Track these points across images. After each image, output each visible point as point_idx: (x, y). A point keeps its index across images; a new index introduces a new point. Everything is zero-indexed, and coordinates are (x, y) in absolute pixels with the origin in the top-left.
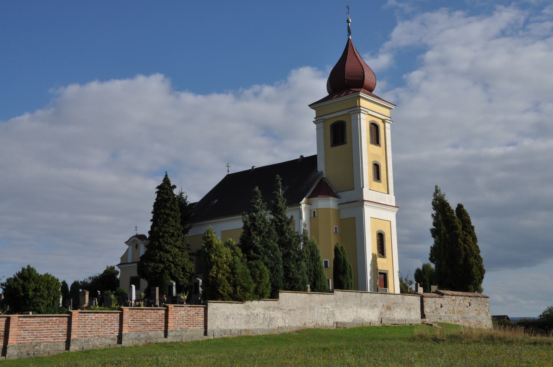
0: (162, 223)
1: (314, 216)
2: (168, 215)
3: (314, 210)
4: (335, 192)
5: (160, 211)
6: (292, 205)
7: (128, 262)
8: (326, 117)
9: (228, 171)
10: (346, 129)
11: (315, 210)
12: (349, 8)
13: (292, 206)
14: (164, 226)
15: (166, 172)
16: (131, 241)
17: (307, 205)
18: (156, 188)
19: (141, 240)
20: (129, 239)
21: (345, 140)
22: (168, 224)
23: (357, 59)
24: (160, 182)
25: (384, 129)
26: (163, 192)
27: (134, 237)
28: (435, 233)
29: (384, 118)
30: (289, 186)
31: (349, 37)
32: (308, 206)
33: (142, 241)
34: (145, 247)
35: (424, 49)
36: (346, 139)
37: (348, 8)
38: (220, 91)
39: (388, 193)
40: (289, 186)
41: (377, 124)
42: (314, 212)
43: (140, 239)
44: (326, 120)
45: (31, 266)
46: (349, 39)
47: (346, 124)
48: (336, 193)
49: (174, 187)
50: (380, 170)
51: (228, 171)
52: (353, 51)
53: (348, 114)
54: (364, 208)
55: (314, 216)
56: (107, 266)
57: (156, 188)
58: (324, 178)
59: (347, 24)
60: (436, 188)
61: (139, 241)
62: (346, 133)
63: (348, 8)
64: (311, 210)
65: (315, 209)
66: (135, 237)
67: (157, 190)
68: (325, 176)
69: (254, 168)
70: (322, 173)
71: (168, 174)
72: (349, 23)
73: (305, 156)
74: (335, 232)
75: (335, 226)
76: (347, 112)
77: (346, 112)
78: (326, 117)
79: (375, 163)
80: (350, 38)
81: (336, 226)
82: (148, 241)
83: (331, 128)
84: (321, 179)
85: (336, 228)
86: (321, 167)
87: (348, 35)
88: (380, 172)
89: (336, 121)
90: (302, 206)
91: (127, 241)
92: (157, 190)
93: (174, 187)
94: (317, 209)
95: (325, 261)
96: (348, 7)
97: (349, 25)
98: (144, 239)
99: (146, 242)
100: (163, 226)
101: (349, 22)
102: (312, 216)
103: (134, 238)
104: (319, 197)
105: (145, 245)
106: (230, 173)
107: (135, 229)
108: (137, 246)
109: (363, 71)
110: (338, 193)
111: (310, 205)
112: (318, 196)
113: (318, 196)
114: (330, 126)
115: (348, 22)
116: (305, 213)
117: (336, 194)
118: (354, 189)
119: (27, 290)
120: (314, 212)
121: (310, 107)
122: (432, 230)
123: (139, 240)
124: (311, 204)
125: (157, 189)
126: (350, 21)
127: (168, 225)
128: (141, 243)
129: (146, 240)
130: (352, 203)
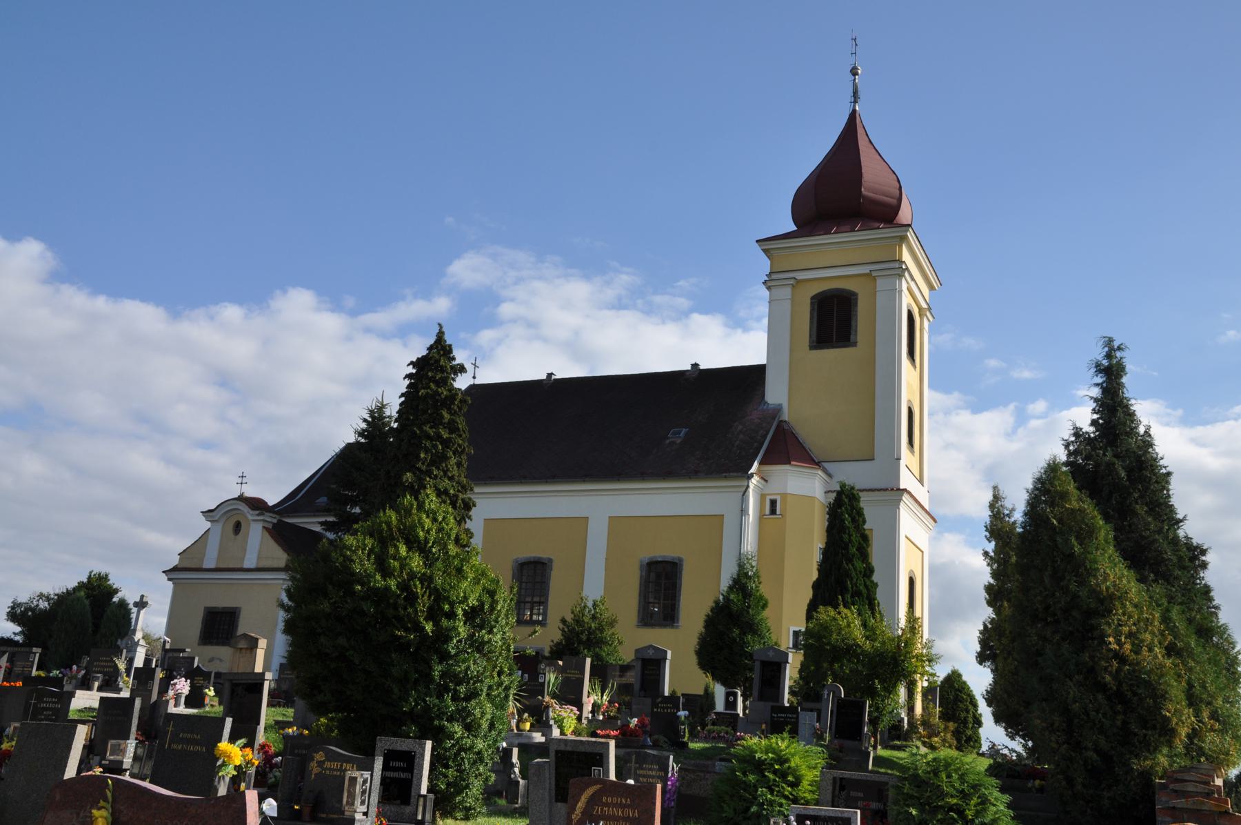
0: (428, 465)
1: (773, 512)
2: (446, 443)
3: (773, 497)
5: (420, 429)
6: (724, 475)
7: (204, 567)
8: (801, 276)
9: (474, 377)
13: (725, 477)
14: (433, 473)
15: (440, 325)
16: (222, 512)
18: (409, 365)
19: (257, 512)
20: (218, 506)
21: (852, 337)
22: (443, 470)
23: (879, 157)
24: (432, 341)
26: (432, 377)
27: (235, 502)
28: (995, 595)
30: (687, 429)
31: (854, 106)
33: (258, 515)
34: (267, 534)
35: (497, 300)
36: (856, 335)
38: (144, 299)
40: (687, 429)
42: (773, 503)
43: (253, 510)
44: (798, 282)
45: (1136, 413)
46: (854, 111)
47: (857, 299)
49: (462, 369)
51: (474, 377)
52: (866, 137)
53: (868, 275)
55: (773, 512)
56: (91, 572)
57: (409, 365)
58: (785, 421)
60: (994, 491)
61: (250, 514)
62: (856, 321)
65: (778, 494)
66: (238, 502)
67: (412, 370)
69: (553, 377)
70: (778, 410)
71: (444, 329)
72: (857, 77)
73: (704, 366)
76: (868, 271)
77: (865, 270)
78: (801, 276)
80: (857, 109)
82: (274, 518)
83: (812, 303)
84: (778, 426)
86: (776, 393)
89: (829, 290)
91: (210, 511)
92: (412, 370)
93: (462, 369)
94: (784, 496)
95: (794, 631)
97: (857, 81)
98: (267, 512)
99: (269, 520)
100: (429, 473)
101: (857, 74)
102: (767, 511)
103: (234, 504)
104: (793, 465)
105: (264, 527)
106: (478, 382)
107: (240, 480)
108: (237, 527)
109: (898, 185)
112: (792, 463)
113: (792, 463)
115: (854, 72)
116: (754, 500)
118: (873, 459)
119: (447, 607)
120: (773, 503)
121: (760, 246)
122: (989, 589)
123: (251, 512)
124: (766, 481)
125: (411, 366)
126: (859, 72)
127: (442, 473)
128: (253, 520)
129: (271, 515)
130: (870, 493)
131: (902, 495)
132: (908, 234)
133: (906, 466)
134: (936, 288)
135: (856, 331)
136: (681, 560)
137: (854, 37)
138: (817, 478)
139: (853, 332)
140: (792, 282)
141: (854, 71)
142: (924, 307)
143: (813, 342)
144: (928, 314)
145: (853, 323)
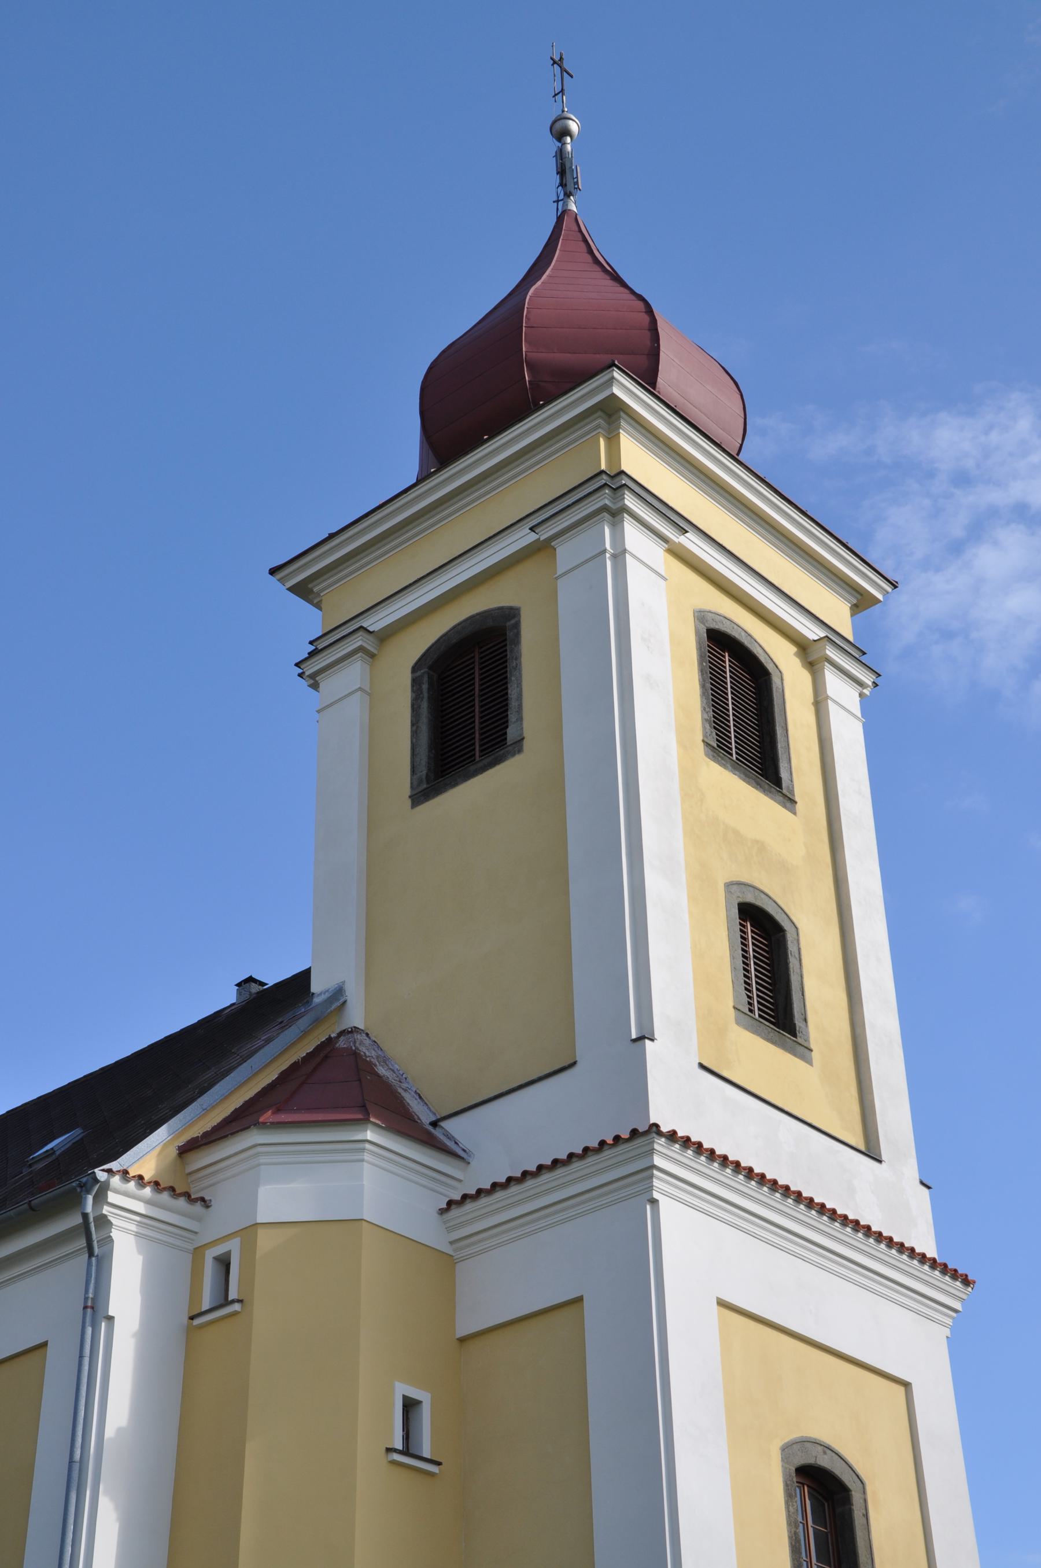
3: (219, 1250)
4: (426, 1118)
8: (376, 622)
10: (518, 658)
11: (234, 1246)
12: (565, 65)
17: (165, 1196)
25: (812, 708)
29: (812, 632)
32: (174, 1213)
36: (520, 719)
37: (563, 70)
39: (872, 1152)
41: (779, 917)
42: (224, 1263)
47: (517, 626)
48: (435, 1124)
50: (793, 962)
54: (654, 1202)
58: (355, 1030)
59: (554, 145)
62: (519, 685)
63: (563, 70)
64: (198, 1253)
68: (356, 1016)
72: (568, 139)
74: (399, 1445)
75: (402, 1389)
79: (801, 1460)
81: (415, 1393)
85: (410, 1406)
87: (558, 201)
88: (794, 979)
90: (112, 1197)
96: (558, 62)
97: (569, 147)
101: (566, 132)
110: (443, 1124)
111: (198, 1208)
114: (414, 669)
117: (437, 1133)
120: (224, 1263)
124: (205, 1202)
131: (651, 1152)
132: (616, 391)
133: (702, 1066)
134: (880, 597)
135: (520, 707)
136: (787, 1449)
137: (557, 58)
138: (367, 1156)
139: (512, 717)
140: (357, 641)
141: (558, 125)
142: (813, 637)
143: (420, 782)
144: (831, 652)
145: (512, 693)
